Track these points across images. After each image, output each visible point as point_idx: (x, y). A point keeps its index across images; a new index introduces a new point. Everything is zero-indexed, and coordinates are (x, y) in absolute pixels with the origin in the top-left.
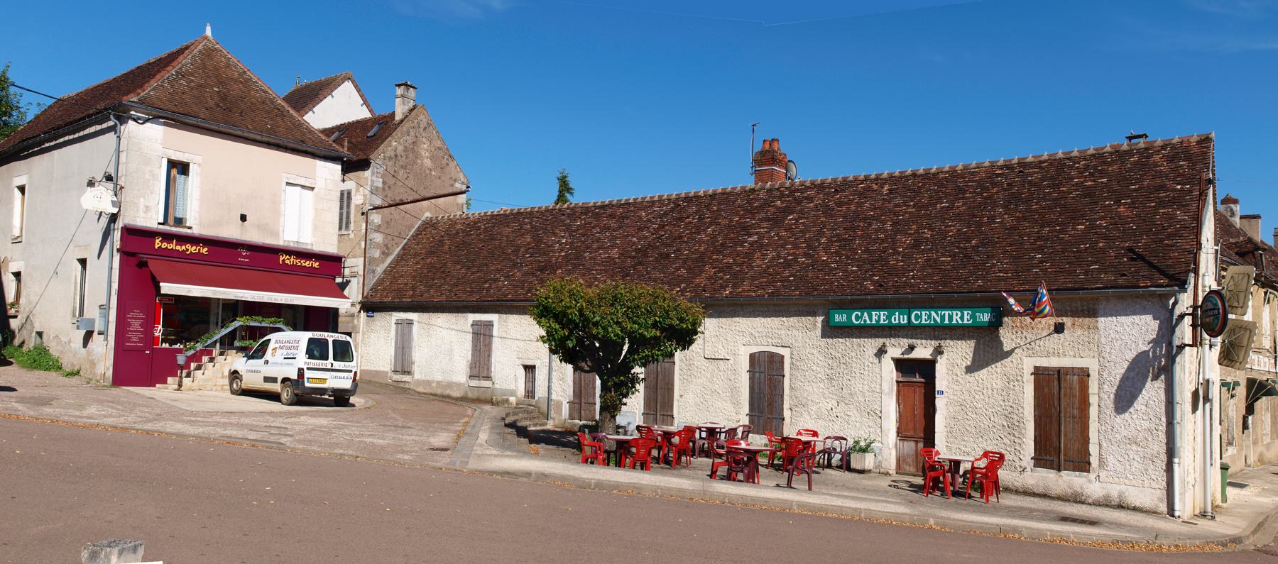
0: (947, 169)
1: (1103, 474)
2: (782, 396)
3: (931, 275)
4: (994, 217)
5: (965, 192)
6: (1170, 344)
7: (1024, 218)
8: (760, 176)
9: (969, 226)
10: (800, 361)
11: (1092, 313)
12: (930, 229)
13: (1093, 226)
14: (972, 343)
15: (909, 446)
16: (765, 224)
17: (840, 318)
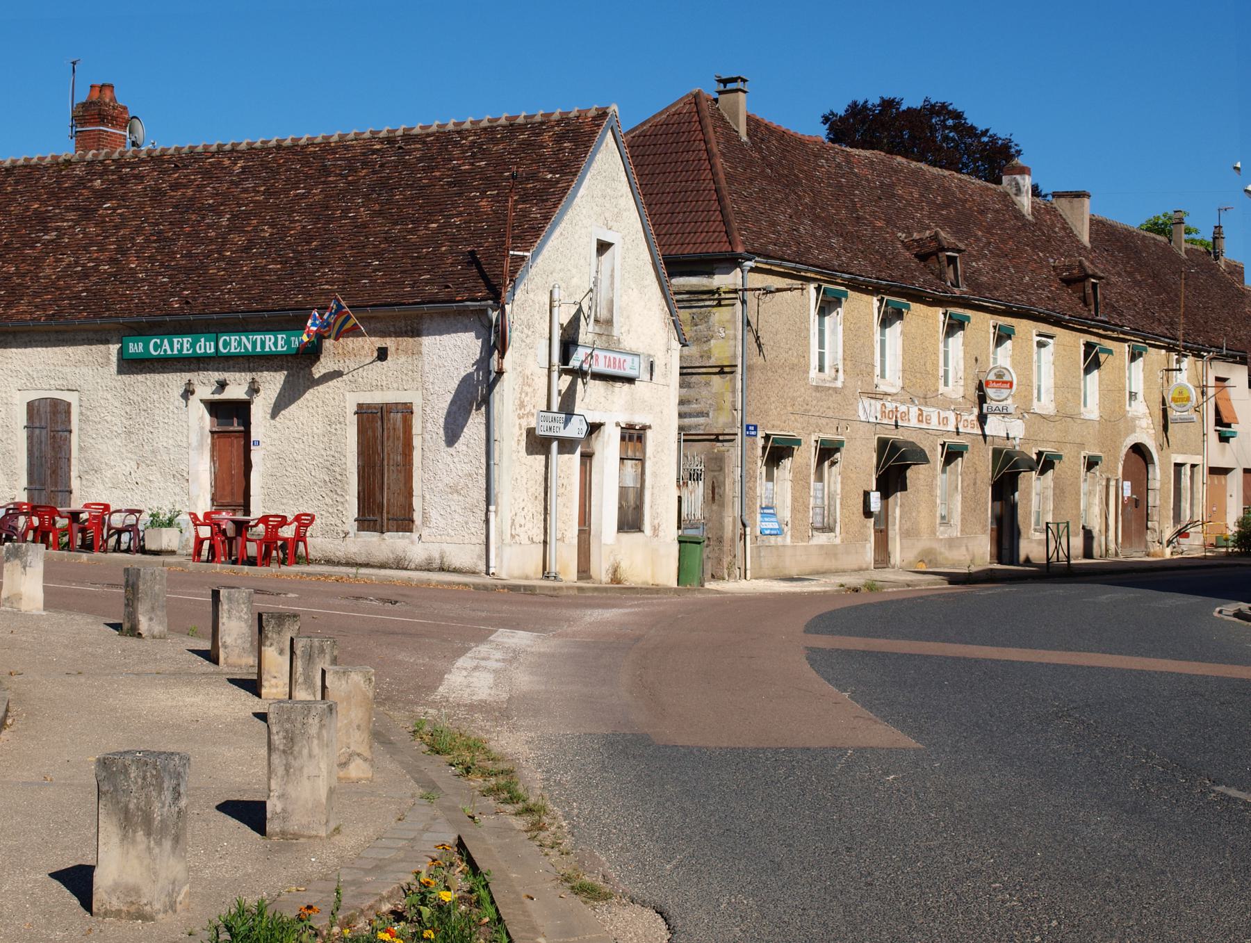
0: (319, 140)
2: (69, 460)
4: (348, 210)
7: (380, 213)
8: (83, 141)
12: (272, 226)
16: (71, 215)
17: (135, 348)
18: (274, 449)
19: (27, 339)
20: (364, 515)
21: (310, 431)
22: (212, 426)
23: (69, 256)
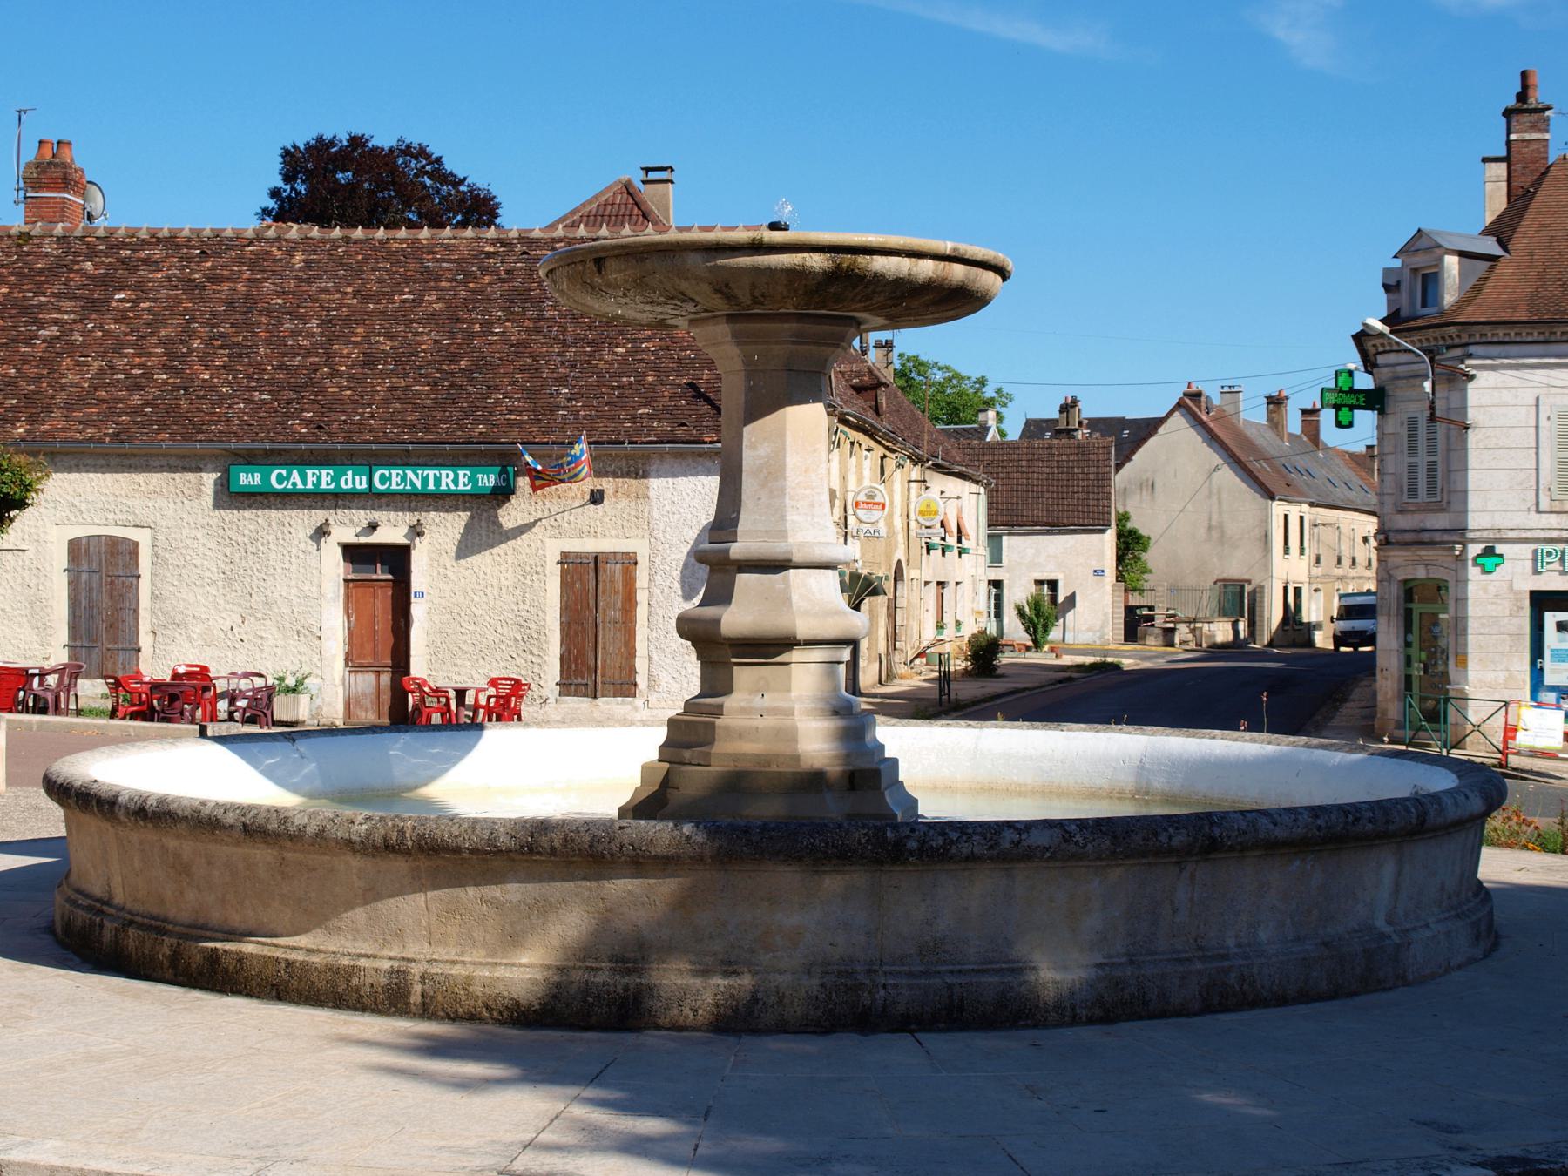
2: (136, 611)
3: (401, 414)
5: (438, 278)
7: (538, 330)
8: (35, 208)
9: (452, 336)
10: (171, 549)
13: (635, 351)
14: (465, 516)
15: (366, 681)
16: (68, 305)
17: (248, 479)
18: (443, 602)
19: (73, 462)
20: (569, 677)
21: (495, 583)
22: (346, 573)
23: (94, 359)
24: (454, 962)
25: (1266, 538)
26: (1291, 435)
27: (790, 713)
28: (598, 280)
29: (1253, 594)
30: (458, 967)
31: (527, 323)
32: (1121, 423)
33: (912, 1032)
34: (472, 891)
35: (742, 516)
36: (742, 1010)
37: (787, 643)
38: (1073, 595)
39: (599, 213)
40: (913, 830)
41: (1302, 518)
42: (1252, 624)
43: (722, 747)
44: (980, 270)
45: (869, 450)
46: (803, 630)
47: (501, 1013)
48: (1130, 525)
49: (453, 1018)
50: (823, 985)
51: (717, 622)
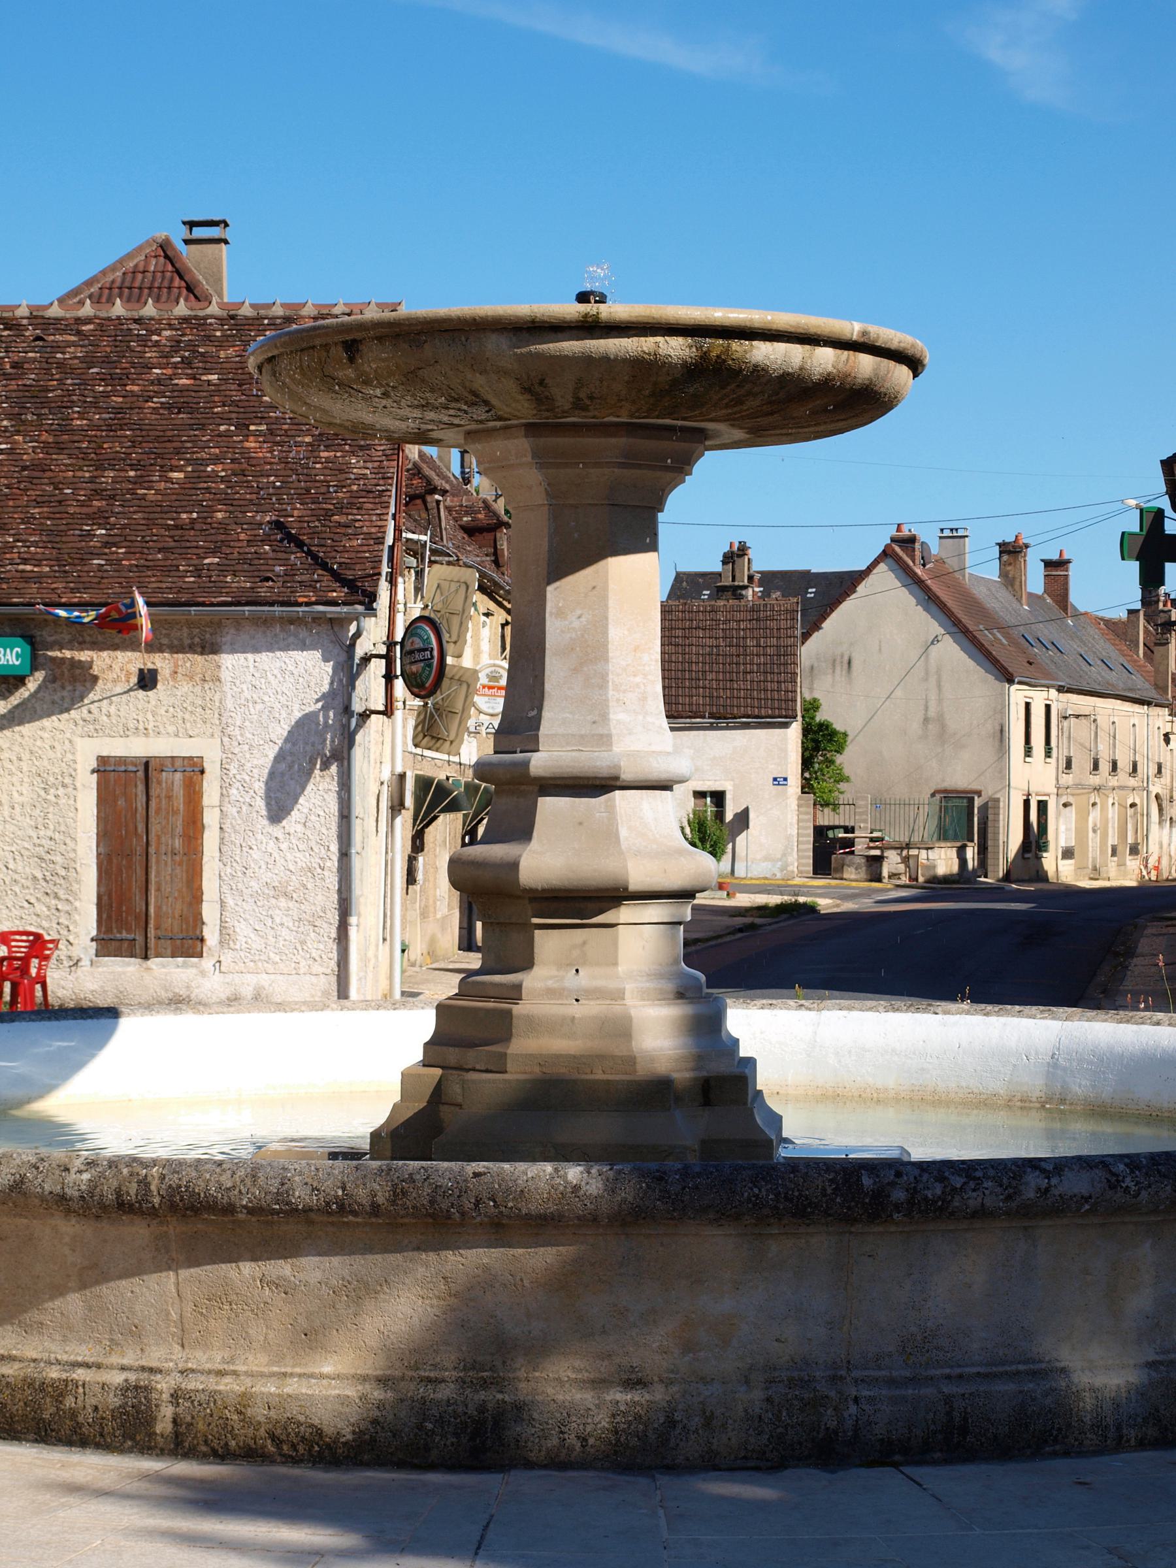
1: (227, 957)
6: (347, 710)
7: (60, 447)
11: (209, 648)
13: (198, 476)
20: (109, 930)
24: (221, 1373)
25: (1002, 734)
26: (1030, 595)
27: (619, 995)
28: (350, 373)
29: (984, 808)
30: (228, 1379)
31: (45, 437)
32: (805, 578)
33: (895, 1465)
34: (248, 1268)
35: (547, 714)
36: (652, 1436)
37: (615, 895)
38: (746, 810)
39: (129, 282)
40: (898, 1174)
41: (1048, 707)
42: (983, 850)
43: (522, 1045)
44: (892, 364)
45: (487, 615)
46: (638, 879)
47: (294, 1447)
48: (820, 717)
49: (221, 1455)
50: (769, 1400)
51: (514, 866)
